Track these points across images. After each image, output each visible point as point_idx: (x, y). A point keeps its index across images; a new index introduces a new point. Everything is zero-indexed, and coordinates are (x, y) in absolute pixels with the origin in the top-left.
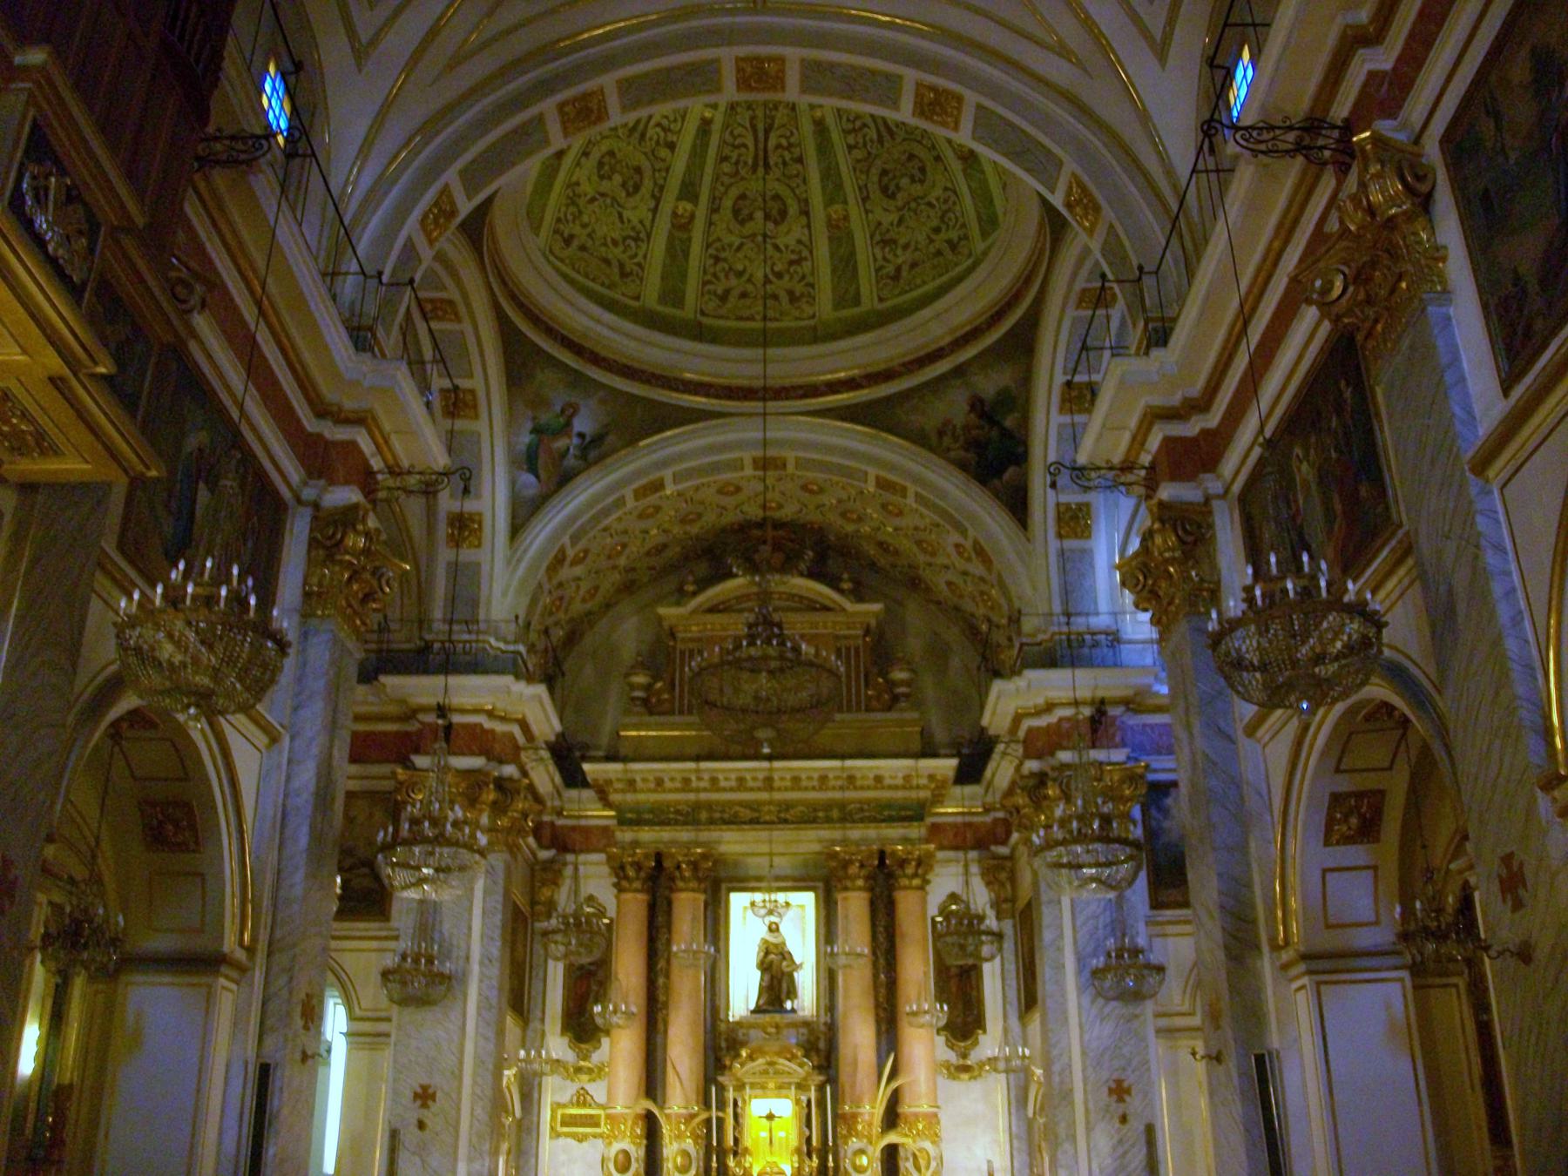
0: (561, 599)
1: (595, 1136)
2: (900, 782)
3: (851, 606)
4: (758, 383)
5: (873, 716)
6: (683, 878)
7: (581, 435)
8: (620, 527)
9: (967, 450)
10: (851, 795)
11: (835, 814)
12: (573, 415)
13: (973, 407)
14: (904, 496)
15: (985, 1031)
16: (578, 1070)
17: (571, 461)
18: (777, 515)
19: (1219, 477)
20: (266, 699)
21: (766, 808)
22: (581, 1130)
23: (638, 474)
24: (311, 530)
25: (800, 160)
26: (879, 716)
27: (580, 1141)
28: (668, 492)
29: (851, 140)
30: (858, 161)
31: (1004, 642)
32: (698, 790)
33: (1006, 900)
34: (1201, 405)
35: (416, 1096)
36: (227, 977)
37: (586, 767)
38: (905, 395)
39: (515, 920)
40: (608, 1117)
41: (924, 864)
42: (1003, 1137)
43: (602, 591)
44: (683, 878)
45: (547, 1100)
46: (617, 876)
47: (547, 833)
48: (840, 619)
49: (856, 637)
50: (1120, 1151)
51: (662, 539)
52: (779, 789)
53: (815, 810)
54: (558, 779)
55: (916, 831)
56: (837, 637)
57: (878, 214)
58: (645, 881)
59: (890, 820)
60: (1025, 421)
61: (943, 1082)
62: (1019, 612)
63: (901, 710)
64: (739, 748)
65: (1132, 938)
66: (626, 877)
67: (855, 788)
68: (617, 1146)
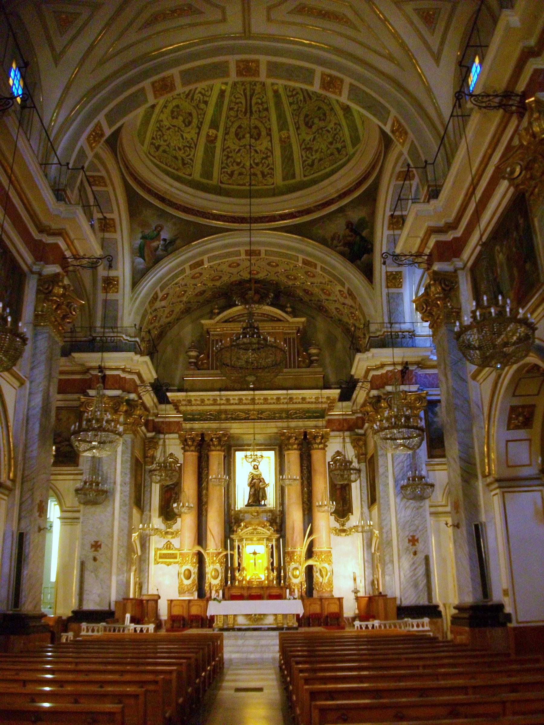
0: (156, 316)
2: (313, 400)
3: (291, 319)
4: (246, 215)
6: (214, 445)
7: (165, 240)
10: (291, 406)
11: (284, 415)
12: (161, 230)
13: (347, 228)
15: (352, 514)
16: (167, 533)
17: (160, 252)
25: (267, 110)
26: (304, 370)
29: (291, 100)
30: (294, 110)
32: (220, 405)
33: (362, 454)
34: (453, 226)
37: (169, 394)
40: (181, 554)
41: (325, 437)
42: (361, 562)
43: (175, 313)
44: (214, 445)
46: (183, 444)
49: (293, 333)
50: (414, 567)
51: (204, 288)
52: (258, 404)
53: (275, 413)
54: (156, 400)
55: (321, 423)
57: (303, 135)
59: (309, 418)
60: (372, 233)
62: (369, 321)
63: (314, 367)
66: (188, 445)
67: (293, 403)
68: (185, 567)
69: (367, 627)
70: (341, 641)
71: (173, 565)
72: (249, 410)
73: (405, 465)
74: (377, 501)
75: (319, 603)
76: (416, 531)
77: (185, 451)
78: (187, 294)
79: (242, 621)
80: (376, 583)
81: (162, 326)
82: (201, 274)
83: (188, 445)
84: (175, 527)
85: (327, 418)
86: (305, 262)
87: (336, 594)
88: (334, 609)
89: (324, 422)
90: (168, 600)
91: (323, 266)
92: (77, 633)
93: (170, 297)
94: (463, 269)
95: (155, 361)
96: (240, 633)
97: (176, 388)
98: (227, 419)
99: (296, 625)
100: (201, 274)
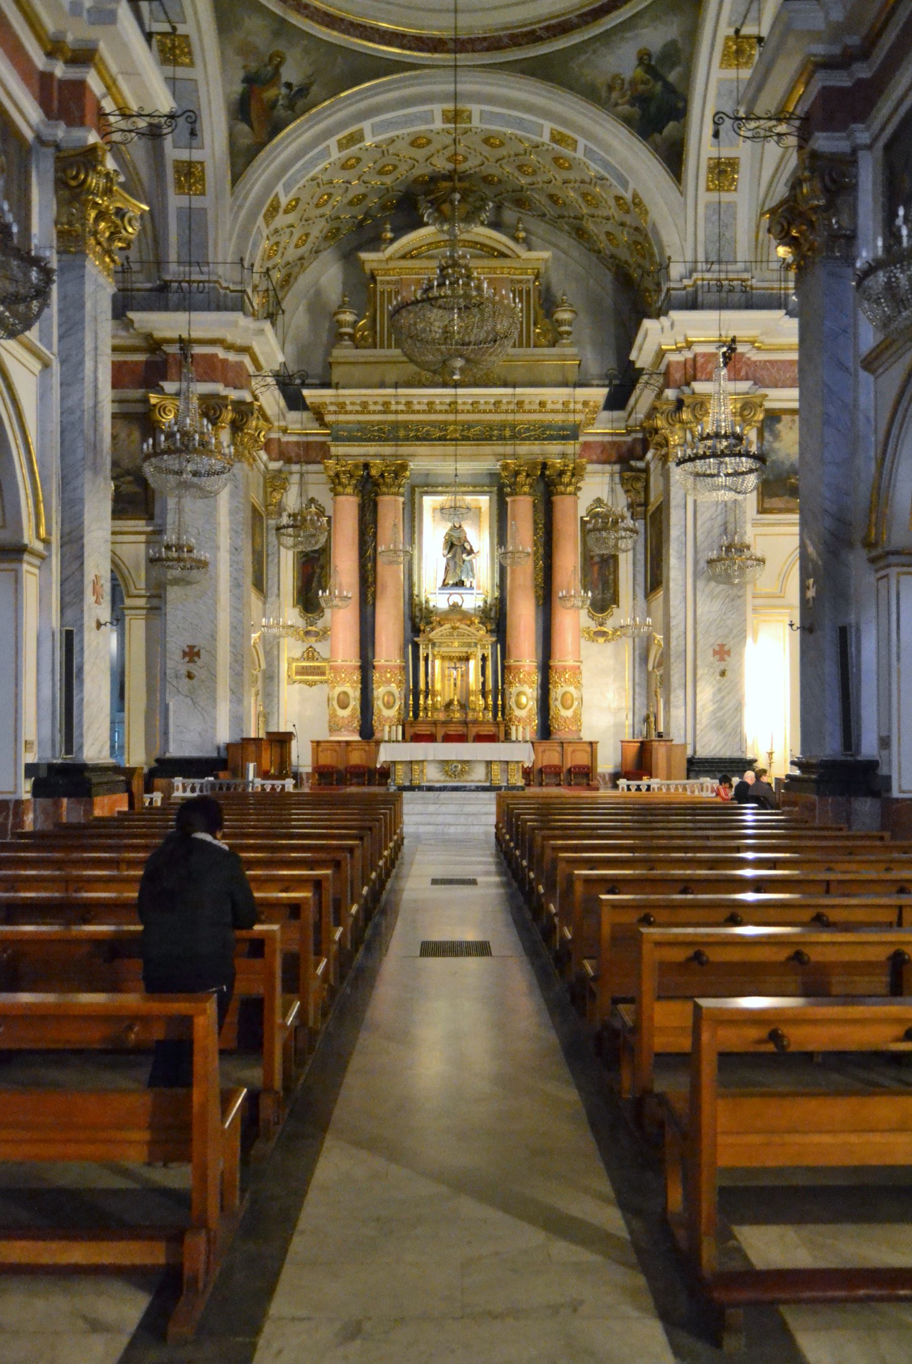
0: (277, 244)
1: (321, 682)
2: (559, 407)
3: (525, 254)
4: (447, 34)
6: (385, 484)
7: (289, 85)
8: (325, 178)
9: (632, 105)
10: (520, 417)
12: (280, 64)
13: (641, 60)
14: (575, 150)
15: (618, 607)
16: (307, 633)
17: (280, 112)
18: (461, 167)
19: (868, 128)
21: (452, 428)
22: (310, 678)
23: (343, 124)
24: (56, 171)
26: (546, 351)
27: (310, 685)
28: (367, 143)
31: (652, 287)
32: (396, 412)
33: (640, 505)
34: (864, 53)
35: (185, 654)
36: (30, 564)
37: (306, 392)
38: (579, 48)
39: (254, 518)
40: (331, 668)
41: (577, 472)
42: (628, 685)
43: (311, 239)
44: (385, 484)
45: (285, 656)
46: (333, 483)
47: (274, 447)
48: (515, 265)
49: (528, 280)
50: (719, 697)
51: (362, 190)
52: (463, 412)
53: (492, 429)
54: (282, 403)
55: (571, 448)
56: (512, 281)
58: (356, 487)
59: (551, 438)
60: (688, 76)
62: (669, 258)
63: (564, 346)
64: (429, 375)
65: (741, 537)
66: (340, 483)
67: (524, 412)
68: (338, 690)
69: (638, 789)
70: (594, 807)
71: (319, 685)
72: (446, 423)
73: (716, 526)
74: (664, 584)
75: (559, 749)
76: (726, 636)
77: (336, 494)
78: (332, 202)
79: (433, 775)
80: (652, 719)
81: (288, 263)
82: (359, 160)
83: (340, 483)
84: (320, 624)
85: (582, 439)
86: (557, 138)
87: (587, 736)
88: (582, 759)
89: (578, 446)
90: (312, 742)
91: (590, 145)
92: (168, 792)
93: (302, 205)
94: (869, 147)
95: (280, 330)
96: (431, 794)
97: (317, 381)
98: (407, 439)
99: (521, 782)
100: (359, 160)
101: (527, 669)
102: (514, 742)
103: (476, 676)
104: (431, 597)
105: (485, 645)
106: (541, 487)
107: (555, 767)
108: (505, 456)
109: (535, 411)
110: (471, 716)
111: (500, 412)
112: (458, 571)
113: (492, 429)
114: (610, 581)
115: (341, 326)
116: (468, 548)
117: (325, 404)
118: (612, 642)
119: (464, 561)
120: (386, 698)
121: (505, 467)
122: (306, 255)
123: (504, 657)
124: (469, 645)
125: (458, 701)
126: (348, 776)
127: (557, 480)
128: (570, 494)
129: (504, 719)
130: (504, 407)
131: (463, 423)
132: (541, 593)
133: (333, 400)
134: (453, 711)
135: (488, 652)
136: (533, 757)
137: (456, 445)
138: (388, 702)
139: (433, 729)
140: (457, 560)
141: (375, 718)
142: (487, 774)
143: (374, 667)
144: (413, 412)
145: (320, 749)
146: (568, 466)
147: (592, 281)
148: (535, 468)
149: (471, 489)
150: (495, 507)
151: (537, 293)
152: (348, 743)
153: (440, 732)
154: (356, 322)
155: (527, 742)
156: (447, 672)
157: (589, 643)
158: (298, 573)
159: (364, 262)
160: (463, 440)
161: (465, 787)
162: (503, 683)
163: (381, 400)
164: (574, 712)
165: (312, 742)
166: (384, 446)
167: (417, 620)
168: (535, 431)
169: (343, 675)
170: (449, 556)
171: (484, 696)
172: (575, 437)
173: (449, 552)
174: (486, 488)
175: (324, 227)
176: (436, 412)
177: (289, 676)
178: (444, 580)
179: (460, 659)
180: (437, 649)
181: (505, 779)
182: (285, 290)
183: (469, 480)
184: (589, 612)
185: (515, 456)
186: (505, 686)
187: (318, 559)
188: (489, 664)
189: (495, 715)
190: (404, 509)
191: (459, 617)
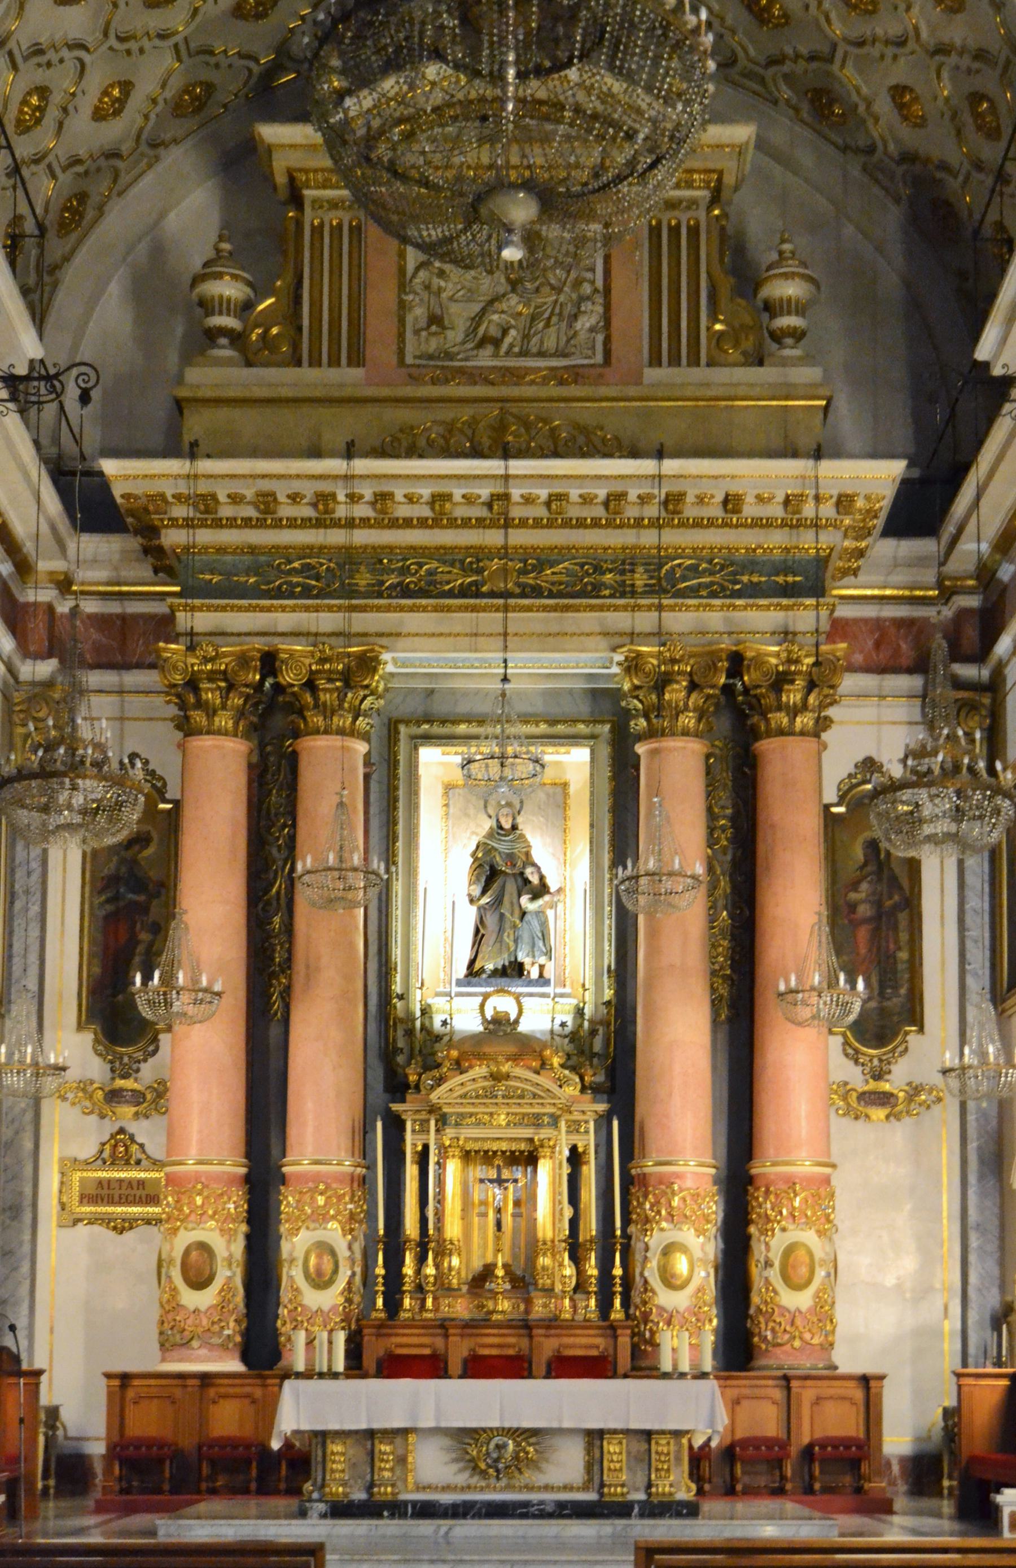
1: (148, 1222)
2: (776, 510)
5: (721, 375)
10: (673, 538)
11: (640, 579)
15: (921, 1030)
16: (114, 1096)
20: (63, 1504)
21: (495, 564)
32: (350, 524)
40: (170, 1179)
42: (949, 1230)
43: (137, 101)
49: (693, 203)
52: (523, 523)
53: (598, 569)
58: (240, 714)
59: (753, 591)
61: (841, 1126)
63: (784, 362)
66: (200, 704)
67: (683, 524)
68: (185, 1238)
71: (143, 1229)
72: (480, 554)
75: (778, 1394)
83: (200, 704)
84: (148, 1072)
101: (689, 1183)
102: (666, 1376)
103: (555, 1202)
104: (439, 1004)
105: (578, 1123)
106: (724, 724)
107: (770, 1443)
108: (633, 636)
109: (711, 523)
110: (540, 1308)
111: (621, 526)
112: (508, 939)
113: (598, 569)
114: (900, 967)
115: (210, 313)
116: (535, 880)
117: (162, 496)
118: (907, 1120)
119: (523, 914)
120: (313, 1261)
121: (633, 665)
122: (125, 148)
123: (628, 1154)
124: (536, 1121)
125: (505, 1266)
126: (206, 1470)
127: (770, 700)
128: (802, 733)
129: (628, 1316)
130: (631, 512)
131: (525, 553)
132: (724, 991)
133: (182, 488)
134: (494, 1295)
135: (588, 1141)
136: (723, 1420)
137: (506, 609)
138: (319, 1273)
139: (439, 1342)
140: (505, 909)
141: (283, 1312)
142: (589, 1467)
143: (283, 1180)
144: (394, 524)
145: (131, 1394)
146: (797, 661)
147: (849, 230)
148: (712, 667)
149: (543, 728)
150: (606, 772)
151: (715, 234)
152: (206, 1379)
153: (459, 1350)
154: (248, 306)
155: (703, 1376)
156: (476, 1197)
157: (847, 1122)
158: (92, 942)
159: (269, 149)
160: (523, 595)
161: (526, 1504)
162: (626, 1221)
163: (310, 490)
164: (817, 1296)
165: (108, 1376)
166: (317, 609)
167: (400, 1059)
168: (712, 573)
169: (199, 1200)
170: (485, 900)
171: (576, 1258)
172: (817, 589)
173: (484, 892)
174: (581, 727)
175: (170, 73)
176: (453, 523)
177: (63, 1206)
178: (472, 963)
179: (514, 1159)
180: (450, 1132)
181: (641, 1480)
182: (74, 237)
183: (539, 707)
184: (846, 1043)
185: (660, 635)
186: (632, 1229)
187: (145, 909)
188: (590, 1172)
189: (605, 1306)
190: (367, 777)
191: (511, 1049)
